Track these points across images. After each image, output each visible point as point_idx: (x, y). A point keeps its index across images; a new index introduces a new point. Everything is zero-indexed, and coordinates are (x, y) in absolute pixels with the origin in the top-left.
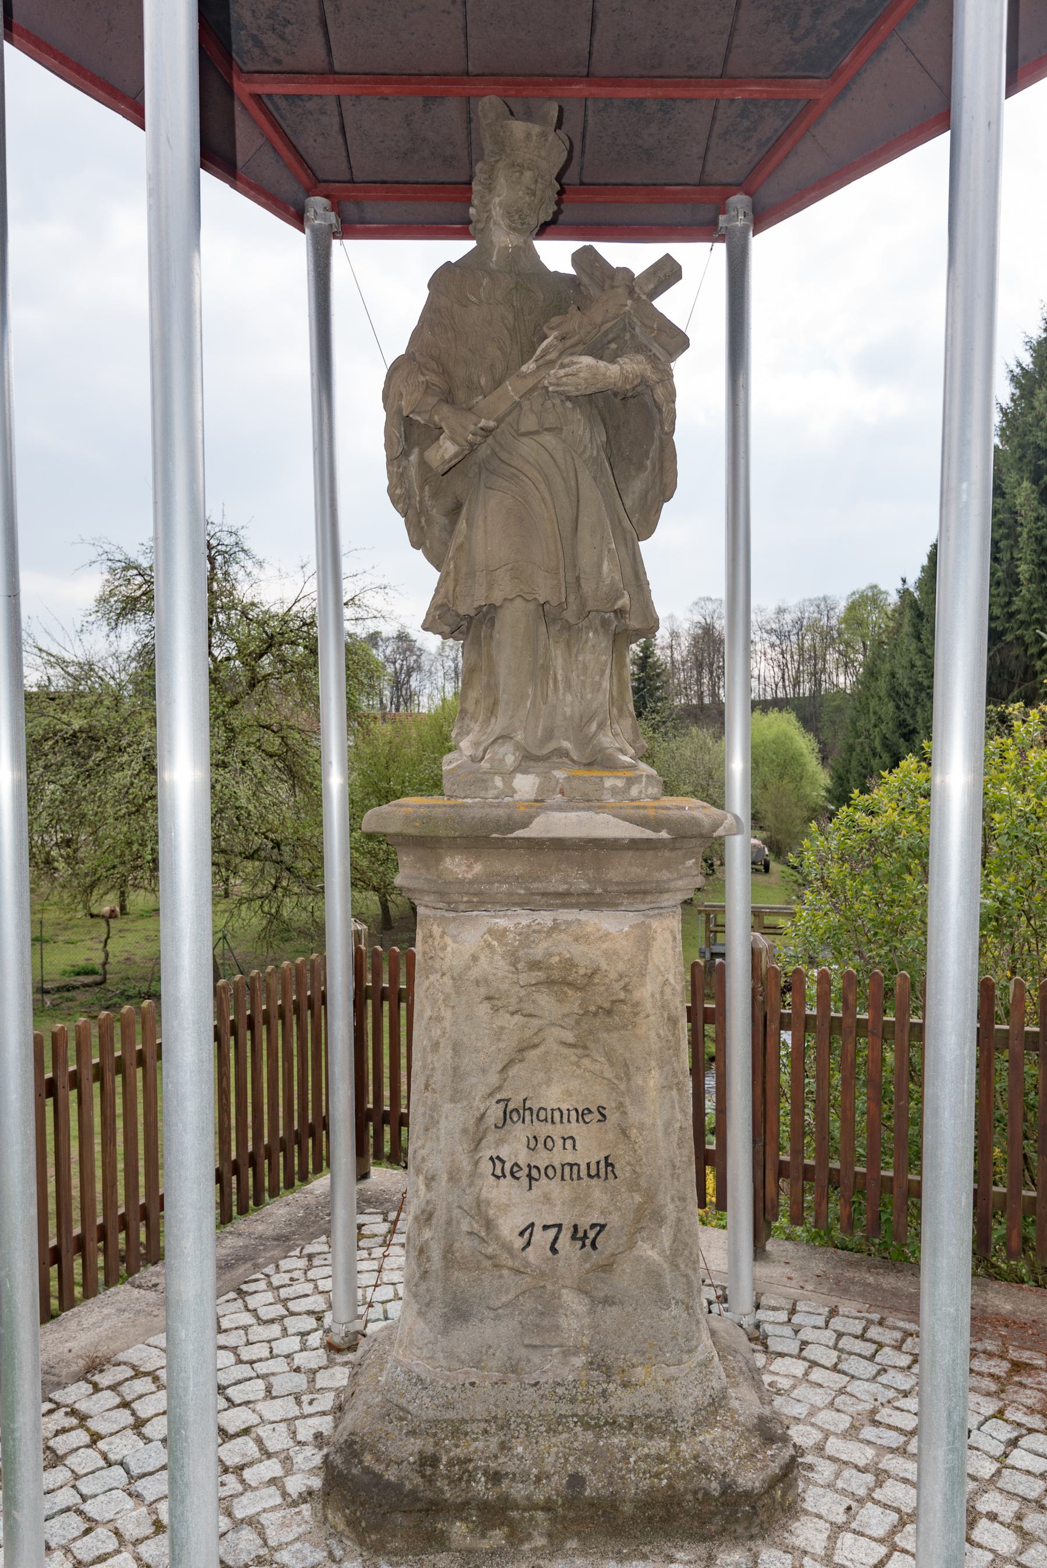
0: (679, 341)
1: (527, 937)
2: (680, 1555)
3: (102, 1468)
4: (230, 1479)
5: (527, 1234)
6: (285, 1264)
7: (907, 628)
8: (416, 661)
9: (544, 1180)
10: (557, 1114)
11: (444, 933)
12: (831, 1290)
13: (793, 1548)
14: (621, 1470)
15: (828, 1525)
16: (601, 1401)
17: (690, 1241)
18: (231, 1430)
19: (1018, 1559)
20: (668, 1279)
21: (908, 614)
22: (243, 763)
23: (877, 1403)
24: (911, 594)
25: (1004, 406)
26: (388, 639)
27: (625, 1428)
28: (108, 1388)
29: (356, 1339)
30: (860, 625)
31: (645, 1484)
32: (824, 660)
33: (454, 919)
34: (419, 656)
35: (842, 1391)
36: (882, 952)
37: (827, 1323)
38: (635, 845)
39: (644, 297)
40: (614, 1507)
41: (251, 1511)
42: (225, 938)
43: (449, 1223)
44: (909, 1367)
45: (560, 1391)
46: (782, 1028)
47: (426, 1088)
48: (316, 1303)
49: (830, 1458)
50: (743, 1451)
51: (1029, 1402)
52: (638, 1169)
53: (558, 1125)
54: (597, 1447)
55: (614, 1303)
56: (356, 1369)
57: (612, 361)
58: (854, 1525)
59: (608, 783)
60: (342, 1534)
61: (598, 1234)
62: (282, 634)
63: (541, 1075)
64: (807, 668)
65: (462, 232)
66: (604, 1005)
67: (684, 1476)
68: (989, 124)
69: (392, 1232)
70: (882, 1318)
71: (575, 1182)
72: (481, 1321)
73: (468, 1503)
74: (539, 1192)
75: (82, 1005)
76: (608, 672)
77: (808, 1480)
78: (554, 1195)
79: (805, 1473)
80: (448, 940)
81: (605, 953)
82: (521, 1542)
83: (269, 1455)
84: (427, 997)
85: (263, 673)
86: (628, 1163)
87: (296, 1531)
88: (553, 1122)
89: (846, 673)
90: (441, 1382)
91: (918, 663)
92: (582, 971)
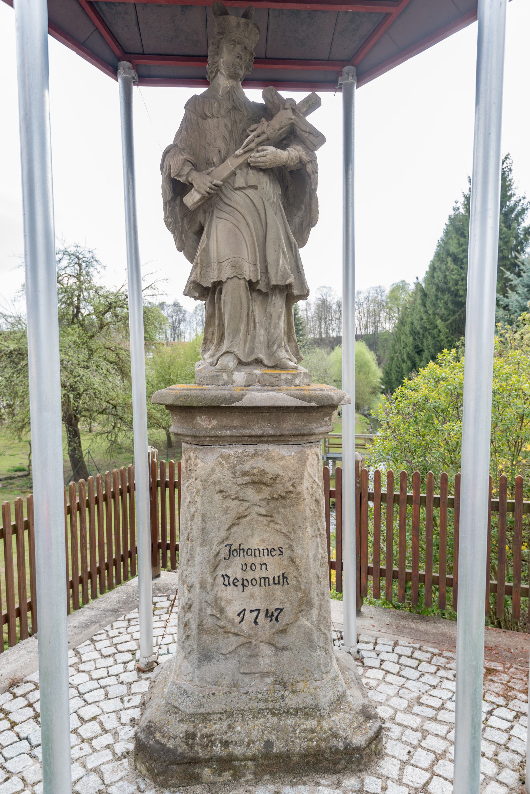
0: (320, 139)
1: (240, 460)
2: (323, 782)
3: (16, 742)
4: (85, 745)
5: (242, 615)
6: (116, 625)
7: (419, 301)
8: (183, 316)
9: (251, 587)
10: (257, 552)
11: (196, 457)
12: (394, 632)
13: (382, 775)
14: (292, 737)
15: (399, 762)
16: (281, 701)
17: (326, 616)
18: (86, 718)
19: (497, 778)
20: (315, 636)
21: (419, 294)
22: (97, 366)
23: (421, 693)
24: (421, 285)
25: (466, 194)
26: (169, 306)
27: (294, 714)
28: (21, 696)
29: (152, 665)
30: (396, 299)
31: (305, 745)
32: (379, 316)
33: (202, 450)
34: (184, 314)
35: (402, 687)
36: (420, 460)
38: (297, 409)
39: (301, 115)
40: (288, 757)
41: (96, 764)
42: (89, 452)
43: (200, 610)
44: (436, 673)
45: (259, 696)
46: (369, 500)
47: (188, 539)
48: (132, 645)
49: (398, 724)
50: (355, 725)
51: (497, 690)
52: (300, 580)
53: (258, 558)
54: (279, 725)
55: (287, 649)
56: (152, 684)
57: (284, 148)
58: (412, 762)
59: (283, 377)
60: (144, 776)
62: (116, 302)
63: (248, 532)
64: (371, 320)
65: (202, 81)
66: (282, 494)
67: (325, 740)
68: (501, 4)
69: (172, 606)
70: (421, 647)
71: (267, 587)
72: (218, 661)
73: (212, 758)
74: (248, 593)
75: (18, 486)
77: (387, 737)
78: (256, 594)
79: (386, 733)
80: (199, 461)
81: (282, 467)
82: (240, 777)
83: (106, 732)
84: (187, 491)
85: (107, 322)
86: (295, 577)
87: (121, 774)
88: (255, 556)
89: (389, 323)
90: (197, 693)
91: (425, 318)
92: (270, 476)
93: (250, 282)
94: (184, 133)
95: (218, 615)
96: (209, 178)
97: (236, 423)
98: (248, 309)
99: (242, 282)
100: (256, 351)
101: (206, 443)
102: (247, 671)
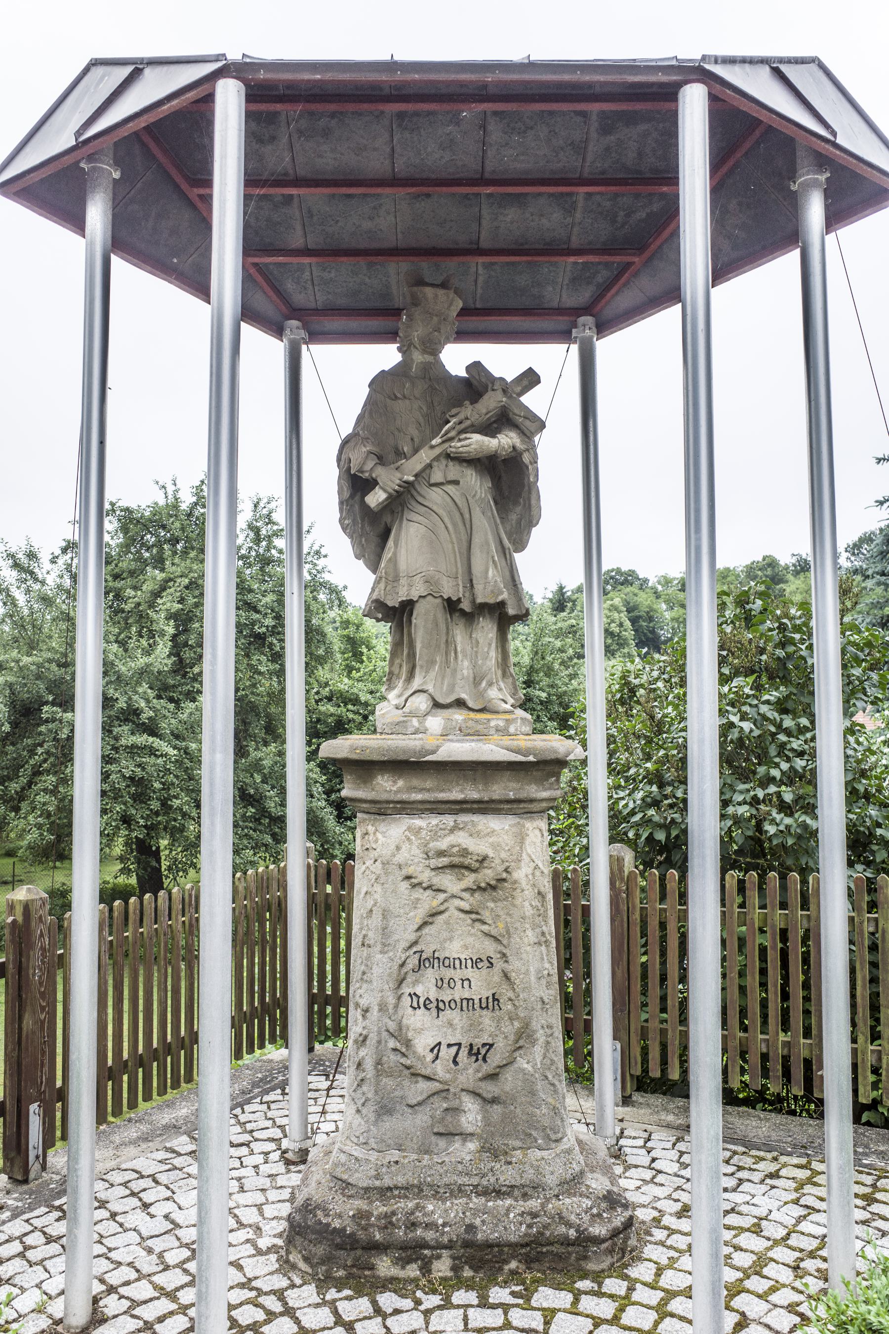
1: (435, 834)
5: (436, 1051)
10: (457, 962)
20: (539, 1085)
35: (679, 1188)
37: (674, 1145)
43: (379, 1042)
47: (363, 945)
57: (493, 436)
61: (488, 1051)
76: (494, 645)
78: (456, 1021)
80: (379, 835)
86: (510, 1000)
92: (475, 858)
93: (449, 600)
94: (367, 419)
95: (404, 1050)
96: (398, 475)
97: (428, 784)
98: (448, 633)
99: (439, 601)
100: (457, 689)
101: (389, 812)
102: (442, 1130)
